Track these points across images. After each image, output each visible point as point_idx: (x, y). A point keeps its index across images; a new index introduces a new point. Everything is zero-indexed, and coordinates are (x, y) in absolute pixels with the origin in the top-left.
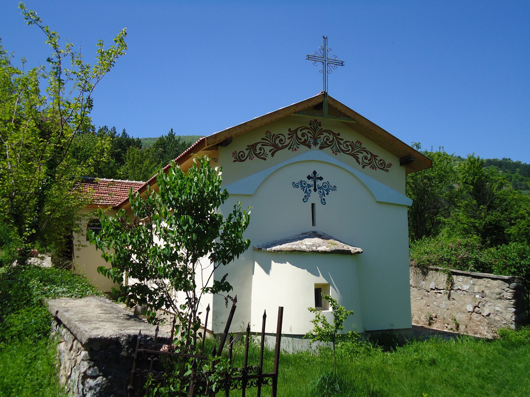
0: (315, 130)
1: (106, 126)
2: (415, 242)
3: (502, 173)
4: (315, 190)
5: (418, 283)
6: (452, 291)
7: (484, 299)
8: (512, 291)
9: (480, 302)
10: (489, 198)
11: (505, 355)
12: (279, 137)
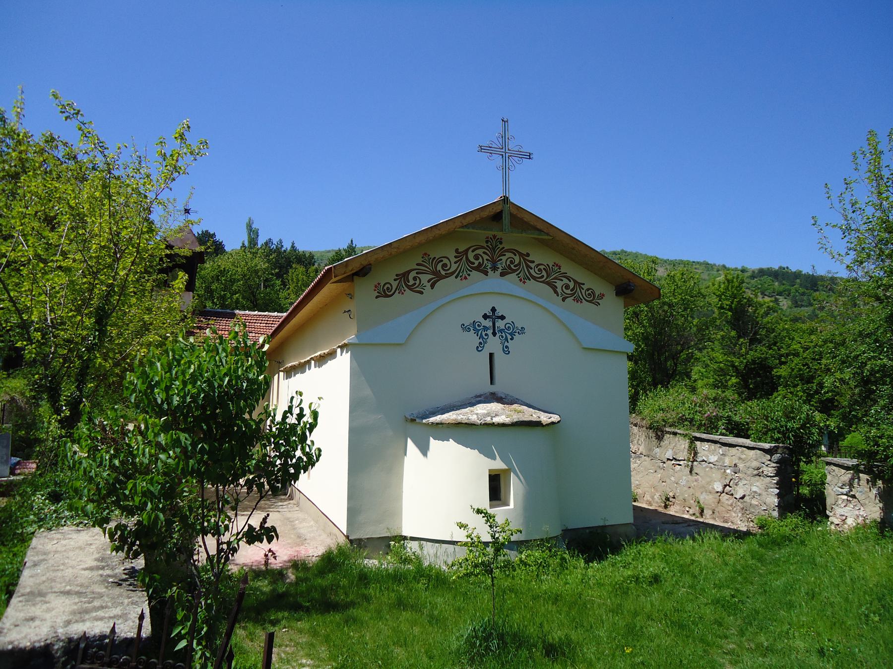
0: (493, 249)
1: (270, 239)
2: (647, 395)
3: (779, 285)
4: (494, 334)
5: (650, 450)
6: (695, 463)
7: (736, 475)
8: (775, 465)
9: (731, 480)
10: (752, 328)
11: (761, 559)
12: (442, 261)
